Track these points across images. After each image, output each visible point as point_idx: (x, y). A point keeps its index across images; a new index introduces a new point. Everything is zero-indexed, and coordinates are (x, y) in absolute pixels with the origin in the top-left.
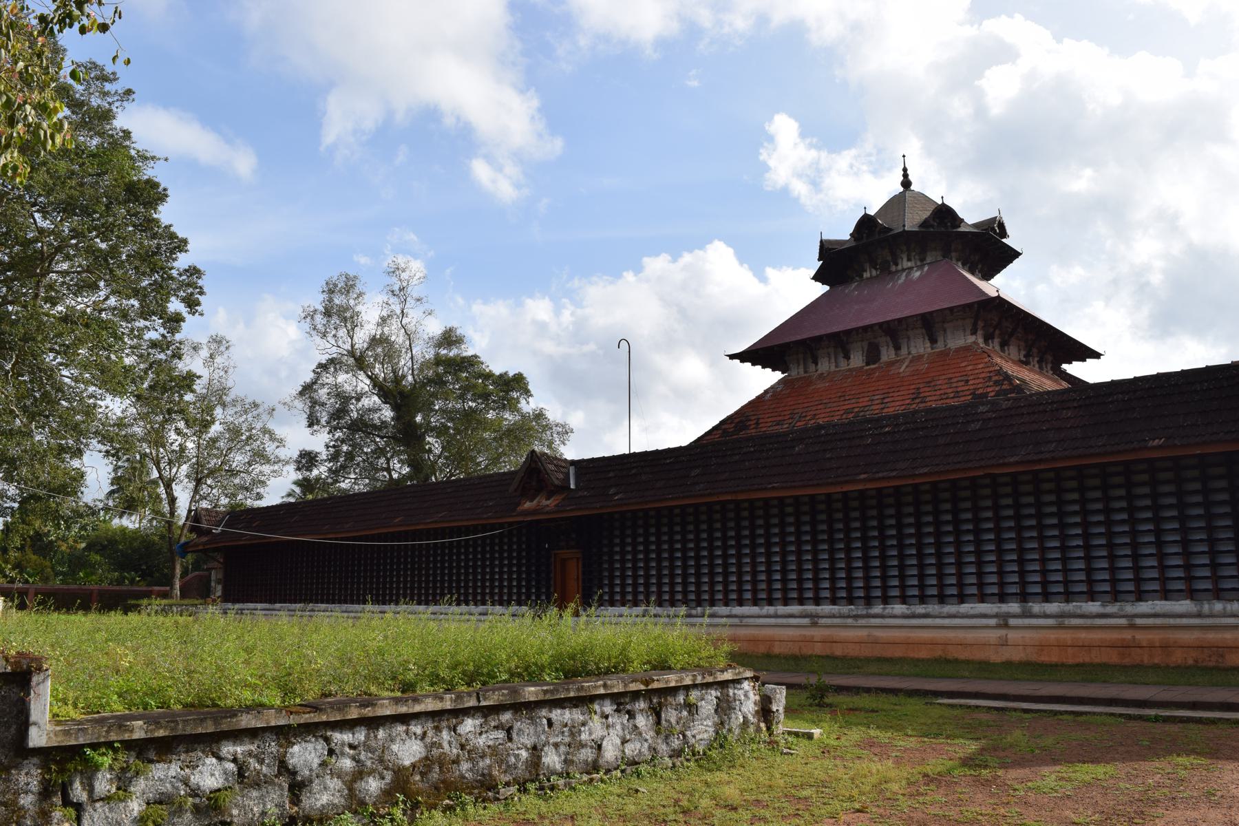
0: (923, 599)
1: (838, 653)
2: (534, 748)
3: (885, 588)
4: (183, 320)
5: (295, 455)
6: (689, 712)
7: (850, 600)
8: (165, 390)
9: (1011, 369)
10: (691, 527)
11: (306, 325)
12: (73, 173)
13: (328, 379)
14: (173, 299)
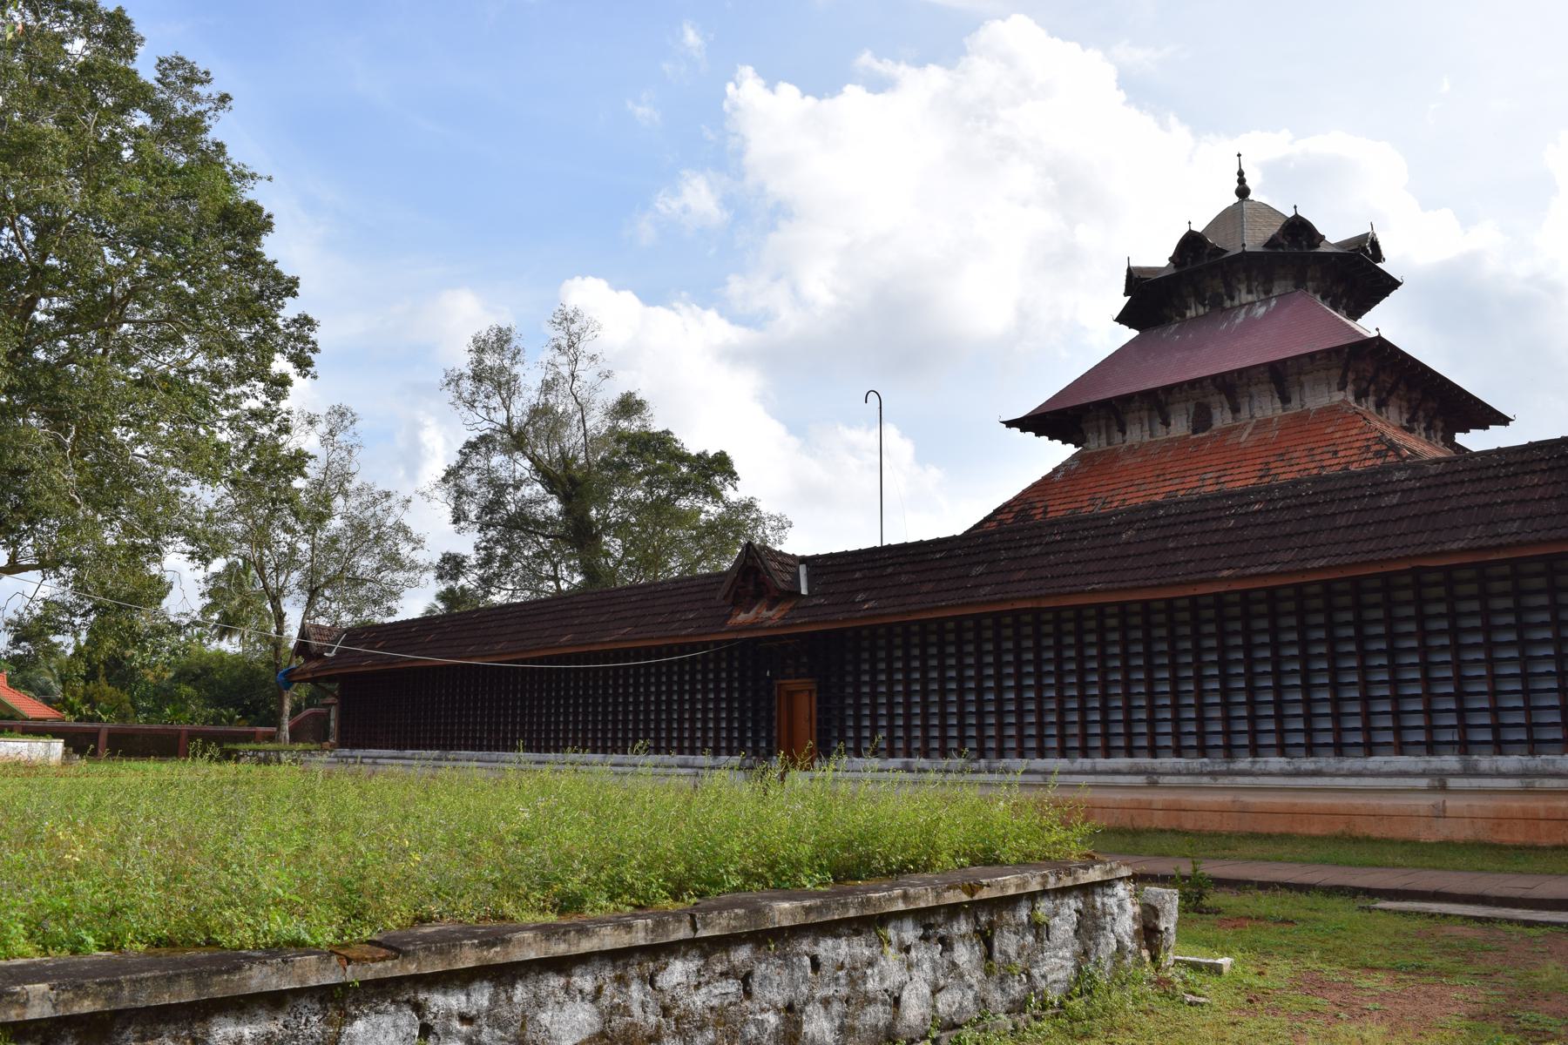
0: (1311, 749)
1: (1188, 826)
2: (790, 1008)
3: (1254, 733)
4: (290, 383)
5: (437, 560)
6: (1037, 936)
7: (1203, 750)
8: (268, 473)
9: (1399, 437)
10: (970, 648)
11: (449, 395)
12: (151, 195)
13: (476, 461)
14: (277, 356)
